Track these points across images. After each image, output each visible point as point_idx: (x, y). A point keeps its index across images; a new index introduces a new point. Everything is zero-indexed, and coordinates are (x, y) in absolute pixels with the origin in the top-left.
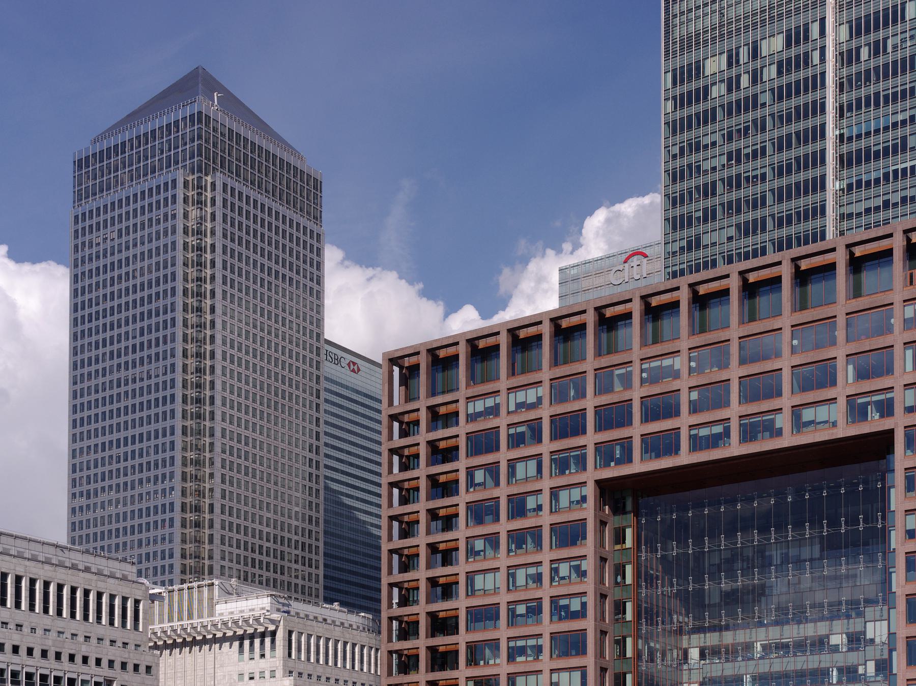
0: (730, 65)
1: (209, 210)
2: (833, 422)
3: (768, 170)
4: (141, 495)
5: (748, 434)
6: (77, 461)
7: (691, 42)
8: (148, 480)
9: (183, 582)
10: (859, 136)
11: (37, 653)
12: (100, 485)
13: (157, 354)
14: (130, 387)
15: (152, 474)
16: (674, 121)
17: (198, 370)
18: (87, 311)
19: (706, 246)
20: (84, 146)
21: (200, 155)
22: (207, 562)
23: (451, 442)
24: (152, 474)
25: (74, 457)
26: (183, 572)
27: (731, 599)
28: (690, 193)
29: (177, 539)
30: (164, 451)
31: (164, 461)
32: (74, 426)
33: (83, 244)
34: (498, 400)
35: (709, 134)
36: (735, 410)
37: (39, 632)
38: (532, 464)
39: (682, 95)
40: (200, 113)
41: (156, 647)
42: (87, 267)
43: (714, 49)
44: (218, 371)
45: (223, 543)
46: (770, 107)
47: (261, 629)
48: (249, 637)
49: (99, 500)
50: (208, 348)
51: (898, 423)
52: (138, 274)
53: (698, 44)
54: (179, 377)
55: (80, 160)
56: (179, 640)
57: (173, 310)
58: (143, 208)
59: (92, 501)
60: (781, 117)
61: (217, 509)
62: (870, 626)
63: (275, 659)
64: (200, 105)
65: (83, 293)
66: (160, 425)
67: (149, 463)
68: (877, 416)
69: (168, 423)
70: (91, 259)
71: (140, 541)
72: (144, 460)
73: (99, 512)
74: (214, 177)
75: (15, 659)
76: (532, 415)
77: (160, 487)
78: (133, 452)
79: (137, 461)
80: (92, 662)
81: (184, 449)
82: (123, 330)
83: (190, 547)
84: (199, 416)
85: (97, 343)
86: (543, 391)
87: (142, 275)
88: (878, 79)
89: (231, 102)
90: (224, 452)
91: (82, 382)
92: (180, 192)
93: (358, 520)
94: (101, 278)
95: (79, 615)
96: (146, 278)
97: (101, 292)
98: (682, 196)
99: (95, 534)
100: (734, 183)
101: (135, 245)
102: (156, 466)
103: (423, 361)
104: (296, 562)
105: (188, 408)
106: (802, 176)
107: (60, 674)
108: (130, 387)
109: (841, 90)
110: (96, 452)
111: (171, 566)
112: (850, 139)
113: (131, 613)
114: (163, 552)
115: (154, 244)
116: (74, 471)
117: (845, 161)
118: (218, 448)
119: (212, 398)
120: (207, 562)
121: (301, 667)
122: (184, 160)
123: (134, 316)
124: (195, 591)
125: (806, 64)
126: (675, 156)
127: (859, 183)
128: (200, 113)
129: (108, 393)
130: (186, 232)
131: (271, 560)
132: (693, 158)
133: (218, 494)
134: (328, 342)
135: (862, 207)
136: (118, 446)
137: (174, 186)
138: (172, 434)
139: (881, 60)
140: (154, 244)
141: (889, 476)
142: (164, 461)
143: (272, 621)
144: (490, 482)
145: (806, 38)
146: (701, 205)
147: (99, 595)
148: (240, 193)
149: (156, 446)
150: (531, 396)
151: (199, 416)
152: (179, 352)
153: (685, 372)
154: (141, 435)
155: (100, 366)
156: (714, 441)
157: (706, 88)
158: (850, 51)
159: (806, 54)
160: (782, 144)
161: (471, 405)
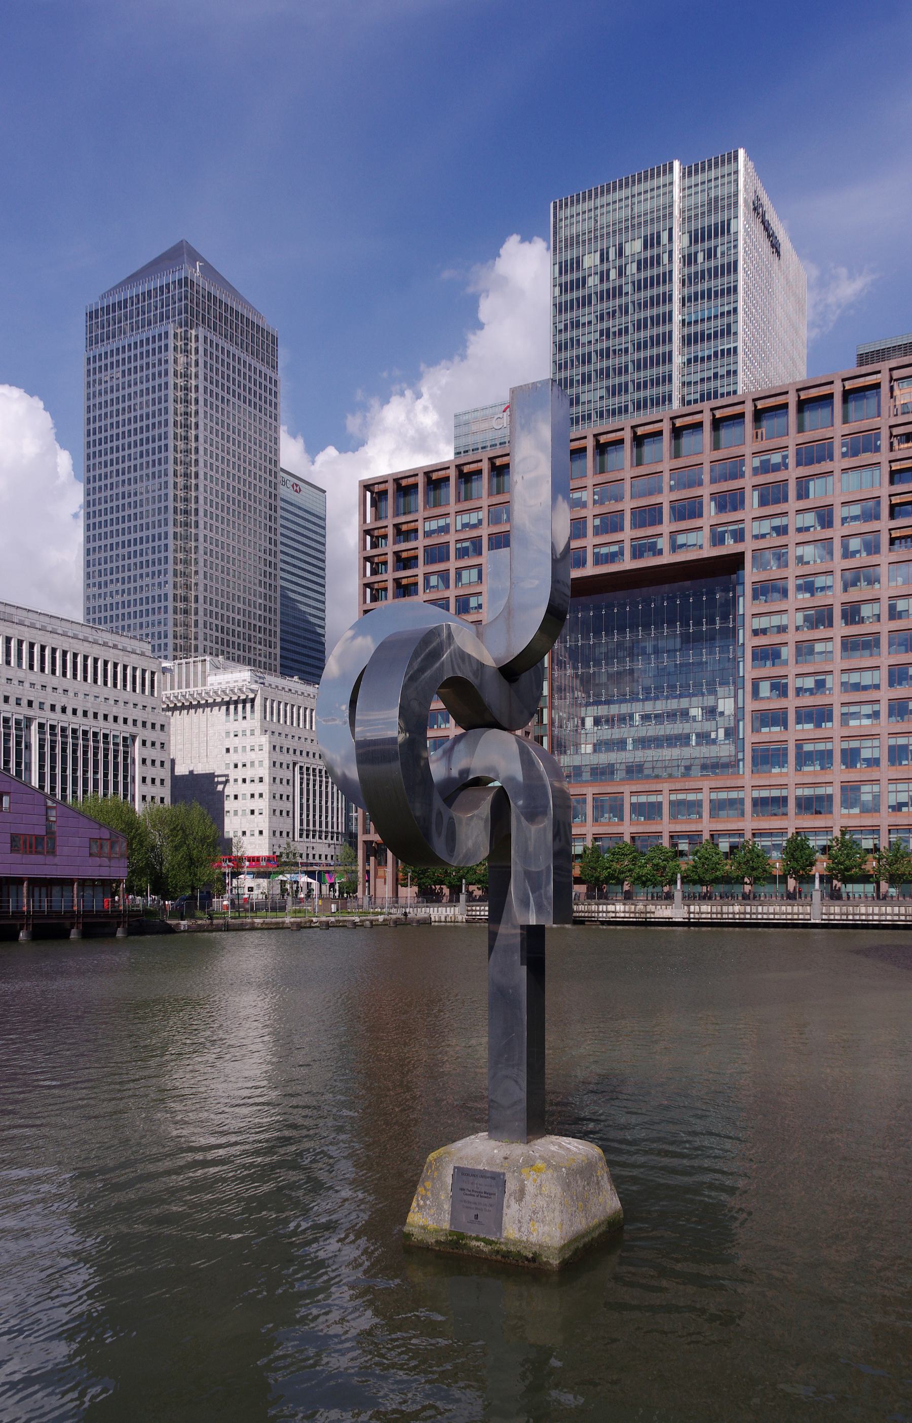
0: (602, 261)
1: (193, 357)
2: (700, 546)
3: (630, 345)
4: (141, 587)
5: (637, 553)
6: (91, 558)
7: (572, 242)
8: (147, 575)
9: (175, 658)
10: (696, 322)
11: (80, 713)
12: (109, 578)
13: (154, 473)
14: (132, 499)
15: (150, 570)
16: (560, 304)
17: (186, 487)
18: (98, 436)
19: (584, 403)
20: (93, 301)
21: (186, 312)
22: (193, 642)
23: (412, 553)
24: (150, 570)
25: (88, 554)
26: (175, 650)
27: (617, 678)
28: (572, 361)
29: (171, 623)
30: (160, 552)
31: (160, 560)
32: (88, 530)
33: (94, 381)
34: (448, 520)
35: (587, 315)
36: (628, 534)
37: (81, 696)
38: (474, 572)
39: (566, 283)
40: (186, 278)
41: (168, 709)
42: (98, 400)
43: (590, 248)
44: (201, 489)
45: (205, 627)
46: (631, 297)
47: (243, 697)
48: (235, 703)
49: (108, 590)
50: (193, 469)
51: (747, 547)
52: (138, 407)
53: (578, 243)
54: (171, 492)
55: (91, 313)
56: (179, 704)
57: (166, 438)
58: (136, 356)
59: (103, 591)
60: (639, 304)
61: (201, 600)
62: (721, 702)
63: (254, 720)
64: (186, 271)
65: (94, 421)
66: (156, 531)
67: (147, 561)
68: (732, 542)
69: (163, 530)
70: (100, 394)
71: (141, 624)
72: (144, 559)
73: (109, 600)
74: (197, 330)
75: (63, 717)
76: (474, 533)
77: (156, 580)
78: (135, 552)
79: (138, 559)
80: (120, 720)
81: (175, 551)
82: (127, 452)
83: (180, 630)
84: (186, 524)
85: (106, 462)
86: (483, 515)
87: (141, 408)
88: (710, 277)
89: (209, 270)
90: (205, 554)
91: (94, 493)
92: (171, 342)
93: (300, 611)
94: (109, 409)
95: (110, 683)
96: (144, 411)
97: (109, 421)
98: (566, 363)
99: (106, 617)
100: (605, 354)
101: (136, 384)
102: (154, 563)
103: (390, 487)
104: (260, 643)
105: (178, 517)
106: (655, 351)
107: (97, 730)
108: (132, 499)
109: (684, 285)
110: (105, 551)
111: (166, 645)
112: (689, 323)
113: (146, 682)
114: (159, 633)
115: (151, 384)
116: (88, 566)
117: (688, 341)
118: (201, 551)
119: (197, 510)
120: (193, 642)
121: (273, 727)
122: (174, 316)
123: (135, 442)
124: (192, 665)
125: (658, 263)
126: (560, 331)
127: (696, 358)
128: (186, 278)
129: (115, 504)
130: (175, 375)
131: (241, 641)
132: (575, 333)
133: (201, 587)
134: (282, 470)
135: (699, 377)
136: (123, 547)
137: (167, 337)
138: (166, 538)
139: (713, 264)
140: (151, 384)
141: (739, 589)
142: (160, 560)
143: (252, 691)
144: (441, 585)
145: (659, 243)
146: (580, 370)
147: (125, 667)
148: (217, 345)
149: (154, 548)
150: (473, 518)
151: (186, 524)
152: (171, 472)
153: (590, 504)
154: (141, 538)
155: (109, 481)
156: (611, 558)
157: (584, 278)
158: (690, 255)
159: (658, 256)
160: (641, 325)
161: (427, 524)
